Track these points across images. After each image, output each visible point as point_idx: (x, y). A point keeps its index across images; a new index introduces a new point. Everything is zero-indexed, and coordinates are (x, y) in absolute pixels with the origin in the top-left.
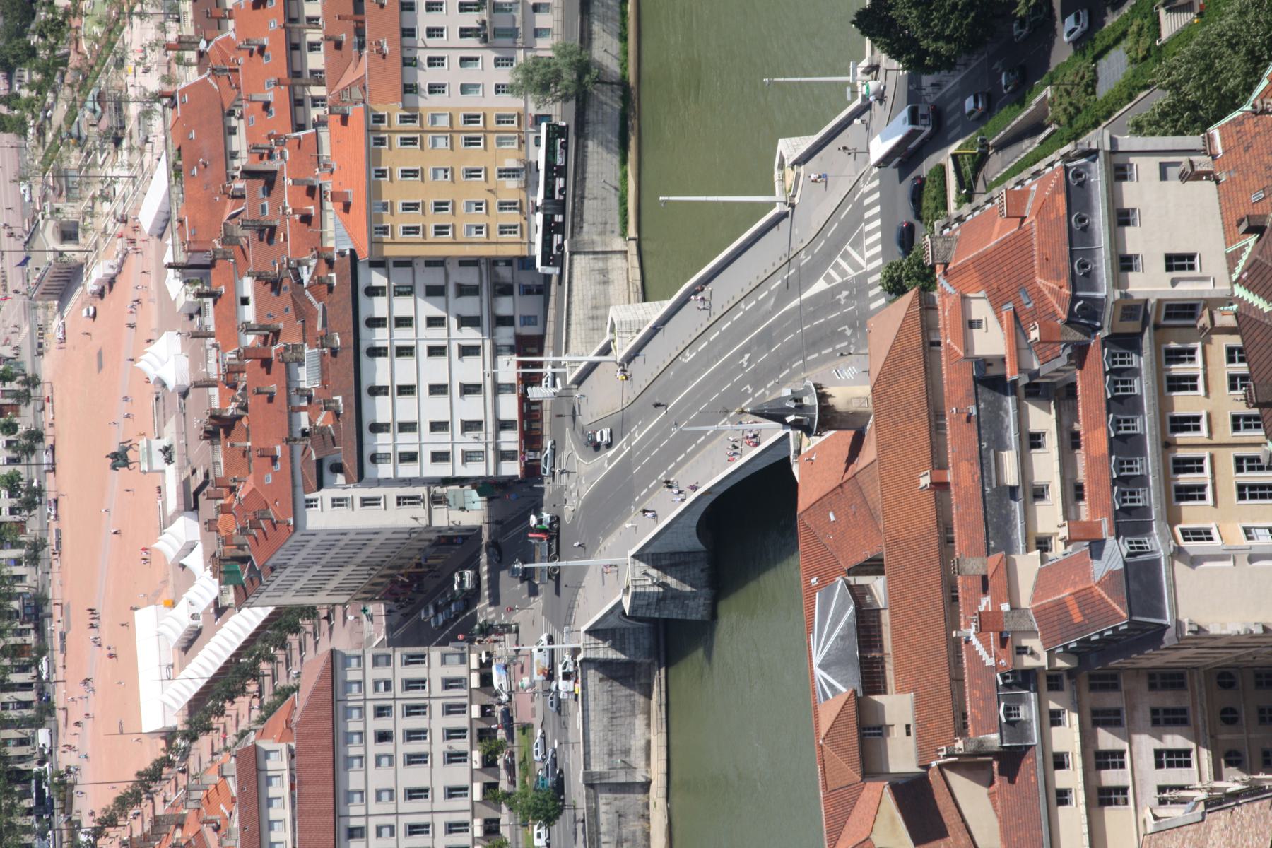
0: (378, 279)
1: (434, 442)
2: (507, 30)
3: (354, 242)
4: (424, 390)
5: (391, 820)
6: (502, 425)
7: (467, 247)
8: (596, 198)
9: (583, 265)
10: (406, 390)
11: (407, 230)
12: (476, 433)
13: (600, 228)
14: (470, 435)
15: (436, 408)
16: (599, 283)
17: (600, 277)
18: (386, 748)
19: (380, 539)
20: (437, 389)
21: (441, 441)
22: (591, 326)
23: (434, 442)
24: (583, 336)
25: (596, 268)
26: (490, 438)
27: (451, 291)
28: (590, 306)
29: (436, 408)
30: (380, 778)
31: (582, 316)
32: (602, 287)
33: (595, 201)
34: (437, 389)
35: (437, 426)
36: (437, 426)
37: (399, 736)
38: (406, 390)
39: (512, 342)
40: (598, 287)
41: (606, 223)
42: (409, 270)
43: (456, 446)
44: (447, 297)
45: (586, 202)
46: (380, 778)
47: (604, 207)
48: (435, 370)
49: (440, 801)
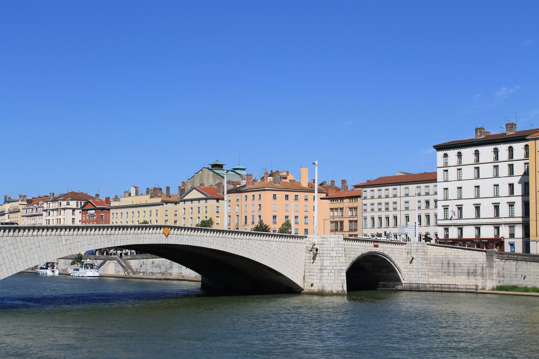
5: (398, 209)
6: (460, 228)
7: (534, 201)
8: (516, 270)
9: (479, 260)
13: (501, 273)
14: (456, 209)
16: (468, 270)
17: (472, 269)
18: (423, 205)
22: (444, 262)
24: (439, 257)
25: (477, 268)
28: (456, 262)
30: (413, 202)
31: (450, 256)
32: (466, 271)
33: (514, 270)
37: (427, 211)
39: (501, 236)
40: (466, 268)
41: (504, 277)
45: (514, 263)
46: (413, 202)
47: (512, 276)
48: (487, 189)
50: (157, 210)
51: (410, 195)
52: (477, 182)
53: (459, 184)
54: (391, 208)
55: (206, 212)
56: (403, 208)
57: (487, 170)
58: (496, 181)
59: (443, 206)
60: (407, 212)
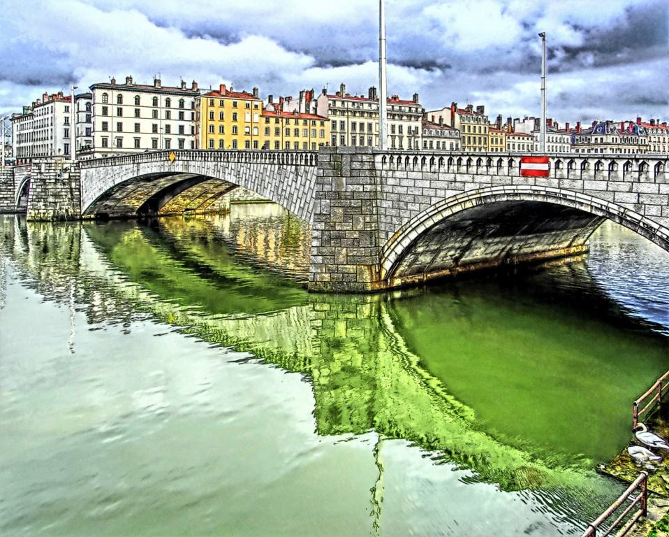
0: (187, 105)
1: (113, 124)
2: (417, 237)
3: (132, 337)
4: (137, 121)
10: (137, 113)
11: (212, 113)
12: (116, 143)
15: (128, 125)
19: (568, 209)
20: (137, 126)
21: (113, 126)
23: (113, 124)
26: (114, 150)
29: (128, 125)
34: (137, 126)
35: (120, 126)
36: (120, 126)
38: (137, 113)
42: (191, 119)
43: (110, 133)
48: (146, 126)
49: (280, 126)
57: (146, 112)
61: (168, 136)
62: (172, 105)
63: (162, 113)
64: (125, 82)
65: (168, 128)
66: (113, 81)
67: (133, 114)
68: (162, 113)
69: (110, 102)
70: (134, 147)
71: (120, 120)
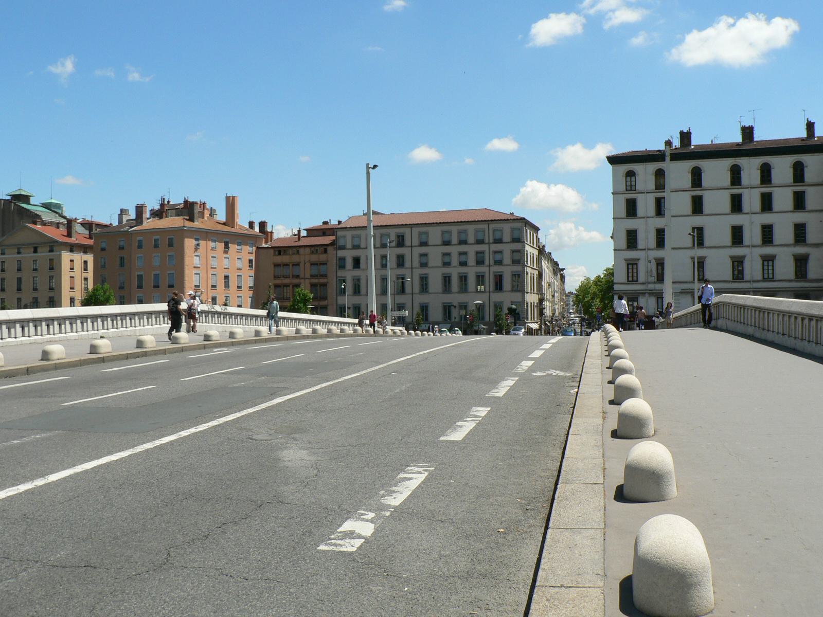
10: (697, 206)
26: (651, 286)
27: (801, 250)
38: (697, 206)
44: (794, 246)
50: (72, 261)
51: (430, 243)
52: (698, 221)
53: (660, 222)
54: (455, 262)
55: (72, 269)
56: (416, 263)
58: (737, 219)
59: (626, 260)
60: (424, 271)
61: (768, 250)
62: (745, 179)
63: (752, 200)
64: (738, 139)
65: (767, 233)
66: (686, 137)
67: (687, 207)
68: (752, 200)
69: (639, 187)
70: (729, 277)
71: (660, 222)
